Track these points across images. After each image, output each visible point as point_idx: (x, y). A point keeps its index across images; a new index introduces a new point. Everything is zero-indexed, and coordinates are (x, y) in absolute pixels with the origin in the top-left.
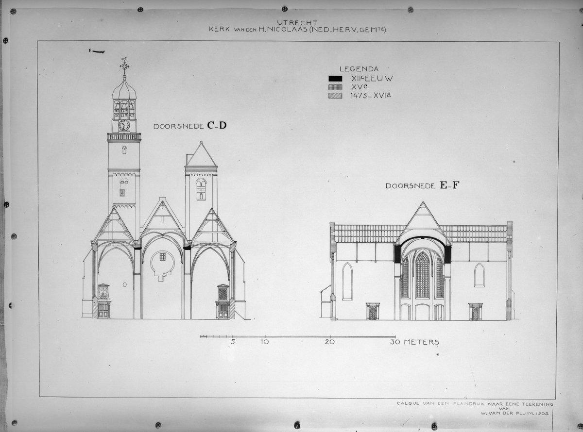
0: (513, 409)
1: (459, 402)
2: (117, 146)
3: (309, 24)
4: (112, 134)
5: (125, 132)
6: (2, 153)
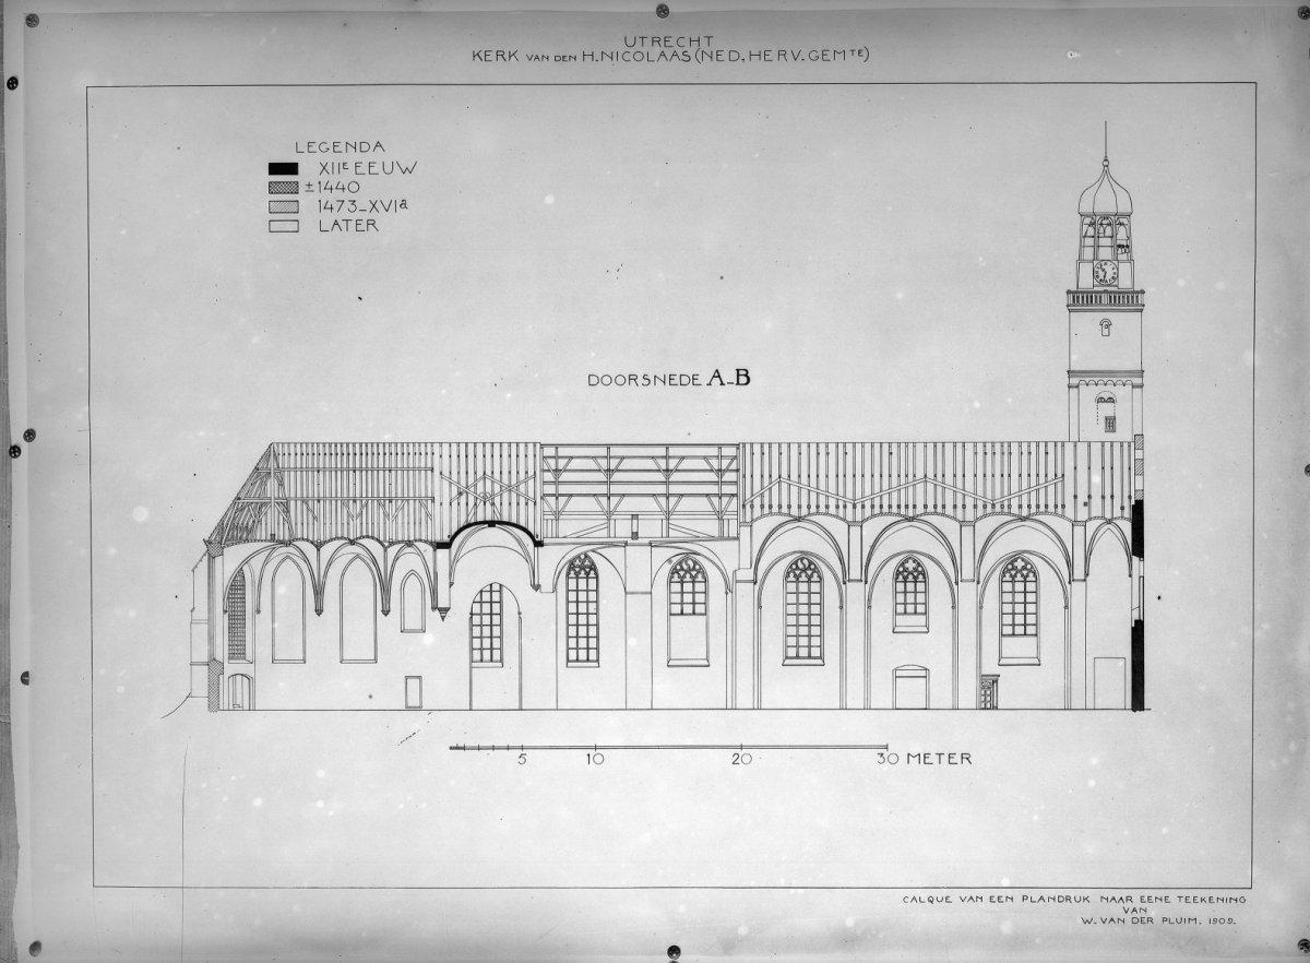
0: (1154, 911)
1: (1035, 895)
2: (1088, 321)
3: (695, 44)
4: (1077, 292)
5: (1109, 289)
6: (6, 337)
